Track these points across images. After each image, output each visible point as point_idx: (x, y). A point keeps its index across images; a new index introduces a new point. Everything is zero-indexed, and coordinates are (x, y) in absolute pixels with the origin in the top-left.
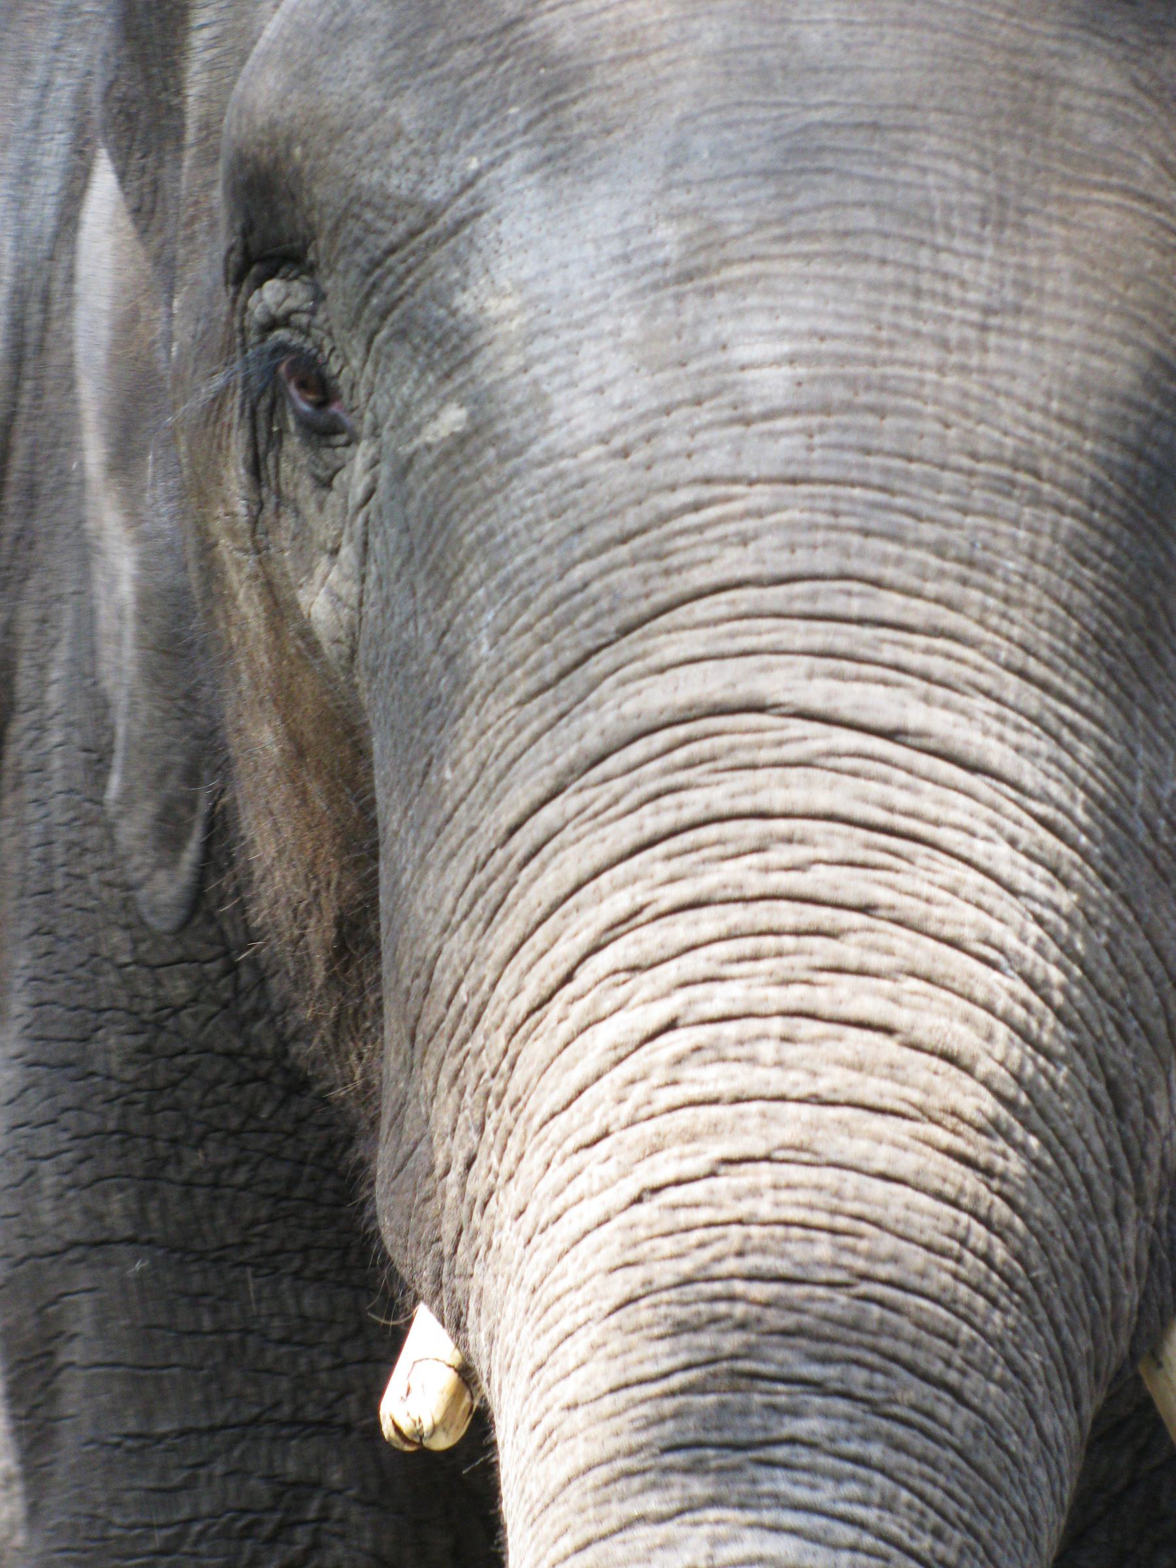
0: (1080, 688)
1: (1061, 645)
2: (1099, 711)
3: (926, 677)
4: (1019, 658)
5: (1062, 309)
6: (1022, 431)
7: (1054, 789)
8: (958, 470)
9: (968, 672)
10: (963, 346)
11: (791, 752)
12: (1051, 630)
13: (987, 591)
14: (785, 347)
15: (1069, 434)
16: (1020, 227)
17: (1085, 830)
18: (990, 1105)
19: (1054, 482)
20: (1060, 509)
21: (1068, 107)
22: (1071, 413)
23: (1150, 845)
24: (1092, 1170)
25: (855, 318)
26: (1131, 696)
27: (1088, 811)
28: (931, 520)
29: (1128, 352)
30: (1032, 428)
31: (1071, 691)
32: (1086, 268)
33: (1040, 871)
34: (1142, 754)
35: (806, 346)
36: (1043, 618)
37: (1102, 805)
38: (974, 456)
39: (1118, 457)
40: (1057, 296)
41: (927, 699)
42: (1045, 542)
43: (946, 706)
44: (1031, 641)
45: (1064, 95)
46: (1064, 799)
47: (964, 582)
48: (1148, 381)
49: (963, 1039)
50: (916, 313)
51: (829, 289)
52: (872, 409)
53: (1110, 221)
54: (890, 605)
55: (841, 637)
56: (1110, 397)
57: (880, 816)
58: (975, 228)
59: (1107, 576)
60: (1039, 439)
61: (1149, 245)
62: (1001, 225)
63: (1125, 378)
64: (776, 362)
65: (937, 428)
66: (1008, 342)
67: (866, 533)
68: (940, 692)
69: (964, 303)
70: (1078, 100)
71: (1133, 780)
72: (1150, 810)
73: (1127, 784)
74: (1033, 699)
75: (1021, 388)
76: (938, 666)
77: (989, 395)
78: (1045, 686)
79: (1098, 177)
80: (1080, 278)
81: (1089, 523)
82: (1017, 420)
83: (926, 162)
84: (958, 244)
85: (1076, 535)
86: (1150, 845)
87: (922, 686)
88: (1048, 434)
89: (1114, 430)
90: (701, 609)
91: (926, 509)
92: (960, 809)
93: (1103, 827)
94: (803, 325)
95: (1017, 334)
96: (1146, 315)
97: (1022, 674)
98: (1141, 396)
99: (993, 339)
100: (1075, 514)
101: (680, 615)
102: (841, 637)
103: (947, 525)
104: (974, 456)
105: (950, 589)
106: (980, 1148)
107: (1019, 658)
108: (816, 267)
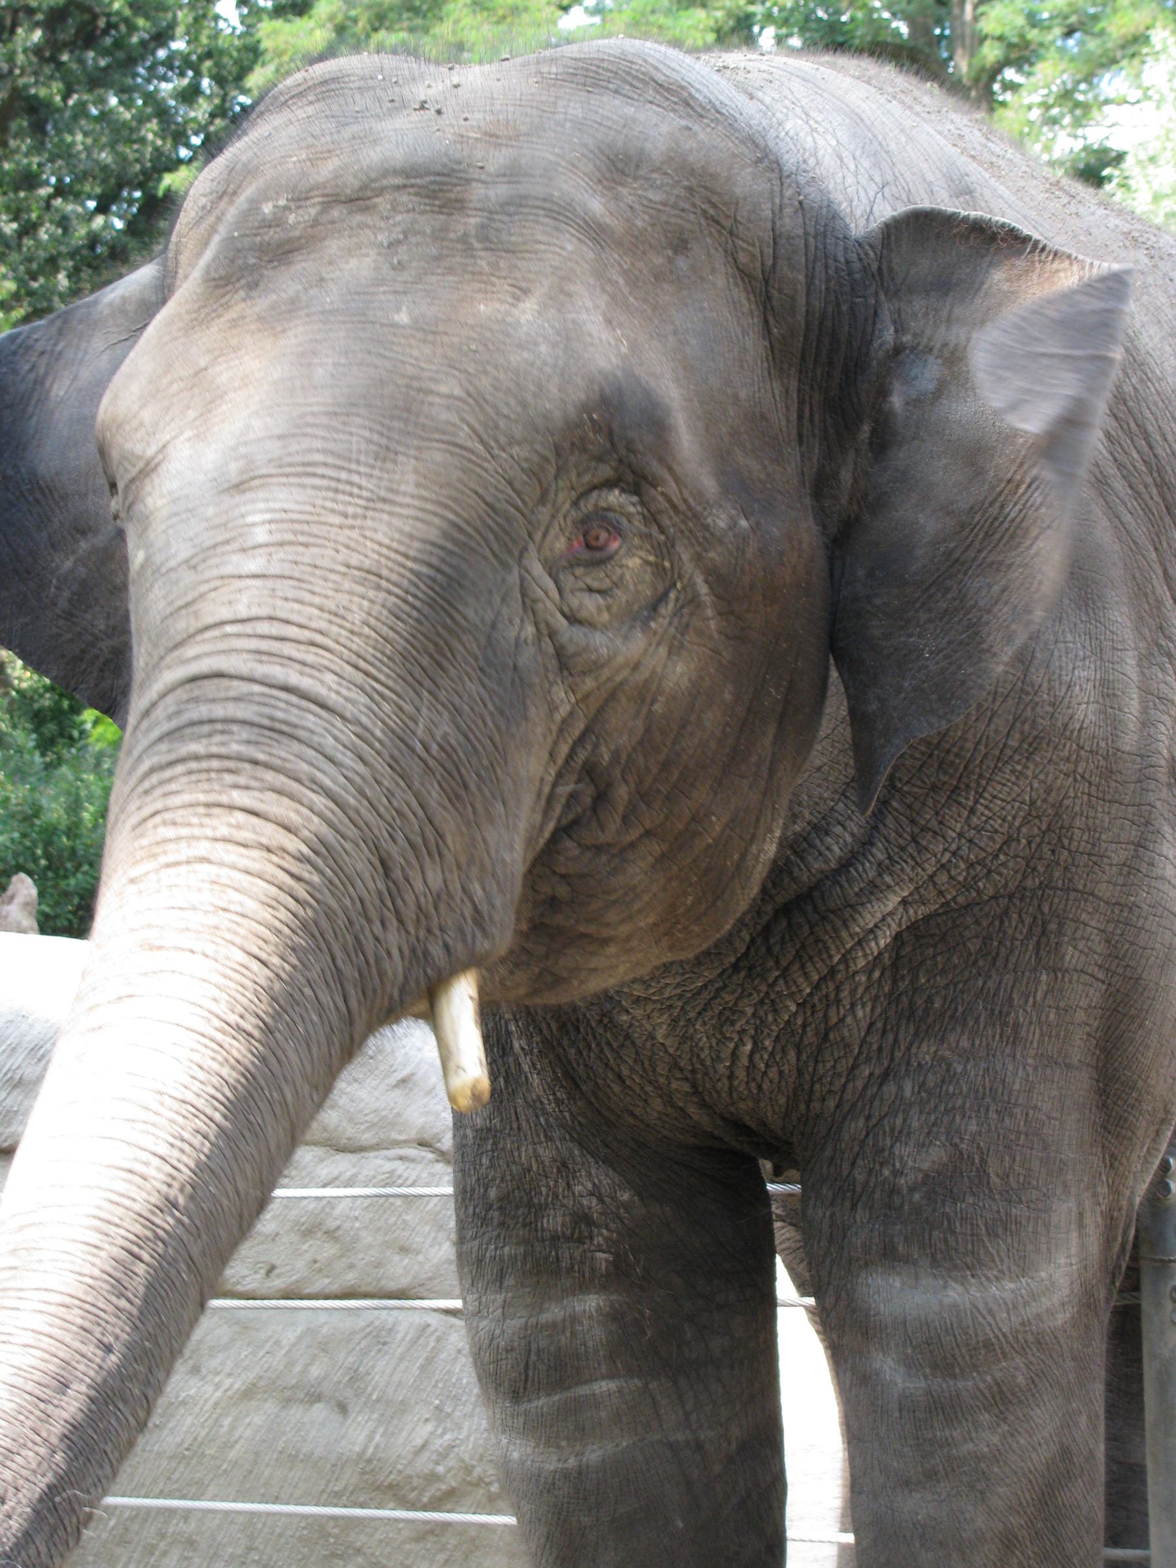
0: (388, 676)
1: (379, 655)
2: (398, 689)
3: (304, 664)
4: (354, 658)
5: (408, 500)
6: (376, 556)
7: (364, 719)
8: (339, 573)
9: (326, 663)
10: (355, 516)
11: (232, 694)
12: (374, 648)
13: (341, 627)
14: (268, 516)
15: (400, 558)
16: (395, 462)
17: (379, 741)
18: (305, 850)
19: (388, 580)
20: (389, 592)
21: (431, 404)
22: (402, 549)
23: (424, 755)
24: (365, 895)
25: (305, 503)
26: (421, 684)
27: (382, 731)
28: (319, 595)
29: (437, 521)
30: (380, 554)
31: (382, 678)
32: (422, 480)
33: (349, 753)
34: (424, 711)
35: (277, 516)
36: (371, 642)
37: (393, 731)
38: (348, 566)
39: (424, 570)
40: (405, 494)
41: (302, 674)
42: (378, 608)
43: (311, 676)
44: (362, 652)
45: (430, 399)
46: (369, 724)
47: (330, 622)
48: (445, 535)
49: (294, 818)
50: (334, 501)
51: (294, 490)
52: (302, 544)
53: (439, 457)
54: (292, 632)
55: (265, 645)
56: (424, 541)
57: (266, 722)
58: (371, 461)
59: (413, 627)
60: (383, 561)
61: (456, 467)
62: (384, 460)
63: (433, 534)
64: (263, 523)
65: (332, 553)
66: (377, 515)
67: (286, 599)
68: (307, 670)
69: (359, 497)
70: (437, 400)
71: (416, 723)
72: (427, 739)
73: (411, 724)
74: (359, 677)
75: (379, 537)
76: (310, 658)
77: (361, 539)
78: (367, 674)
79: (437, 436)
80: (418, 485)
81: (405, 601)
82: (373, 551)
83: (354, 430)
84: (362, 469)
85: (395, 605)
86: (424, 755)
87: (298, 666)
88: (388, 558)
89: (426, 558)
90: (208, 635)
91: (317, 589)
92: (310, 721)
93: (392, 740)
94: (277, 506)
95: (382, 511)
96: (450, 503)
97: (356, 667)
98: (441, 541)
99: (370, 513)
100: (397, 596)
101: (199, 638)
102: (265, 645)
103: (326, 597)
104: (348, 566)
105: (323, 625)
106: (295, 867)
107: (354, 658)
108: (292, 480)
